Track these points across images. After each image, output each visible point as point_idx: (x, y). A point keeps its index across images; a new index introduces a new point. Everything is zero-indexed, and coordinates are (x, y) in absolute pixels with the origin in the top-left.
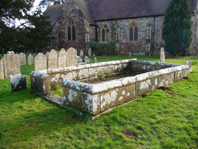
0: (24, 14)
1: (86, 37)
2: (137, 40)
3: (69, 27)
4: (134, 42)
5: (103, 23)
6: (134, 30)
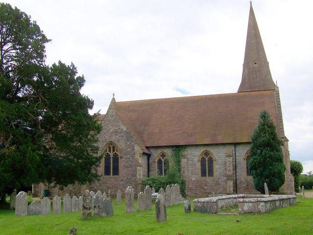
0: (18, 50)
1: (138, 172)
2: (213, 176)
3: (108, 156)
4: (208, 179)
5: (159, 151)
6: (112, 159)
